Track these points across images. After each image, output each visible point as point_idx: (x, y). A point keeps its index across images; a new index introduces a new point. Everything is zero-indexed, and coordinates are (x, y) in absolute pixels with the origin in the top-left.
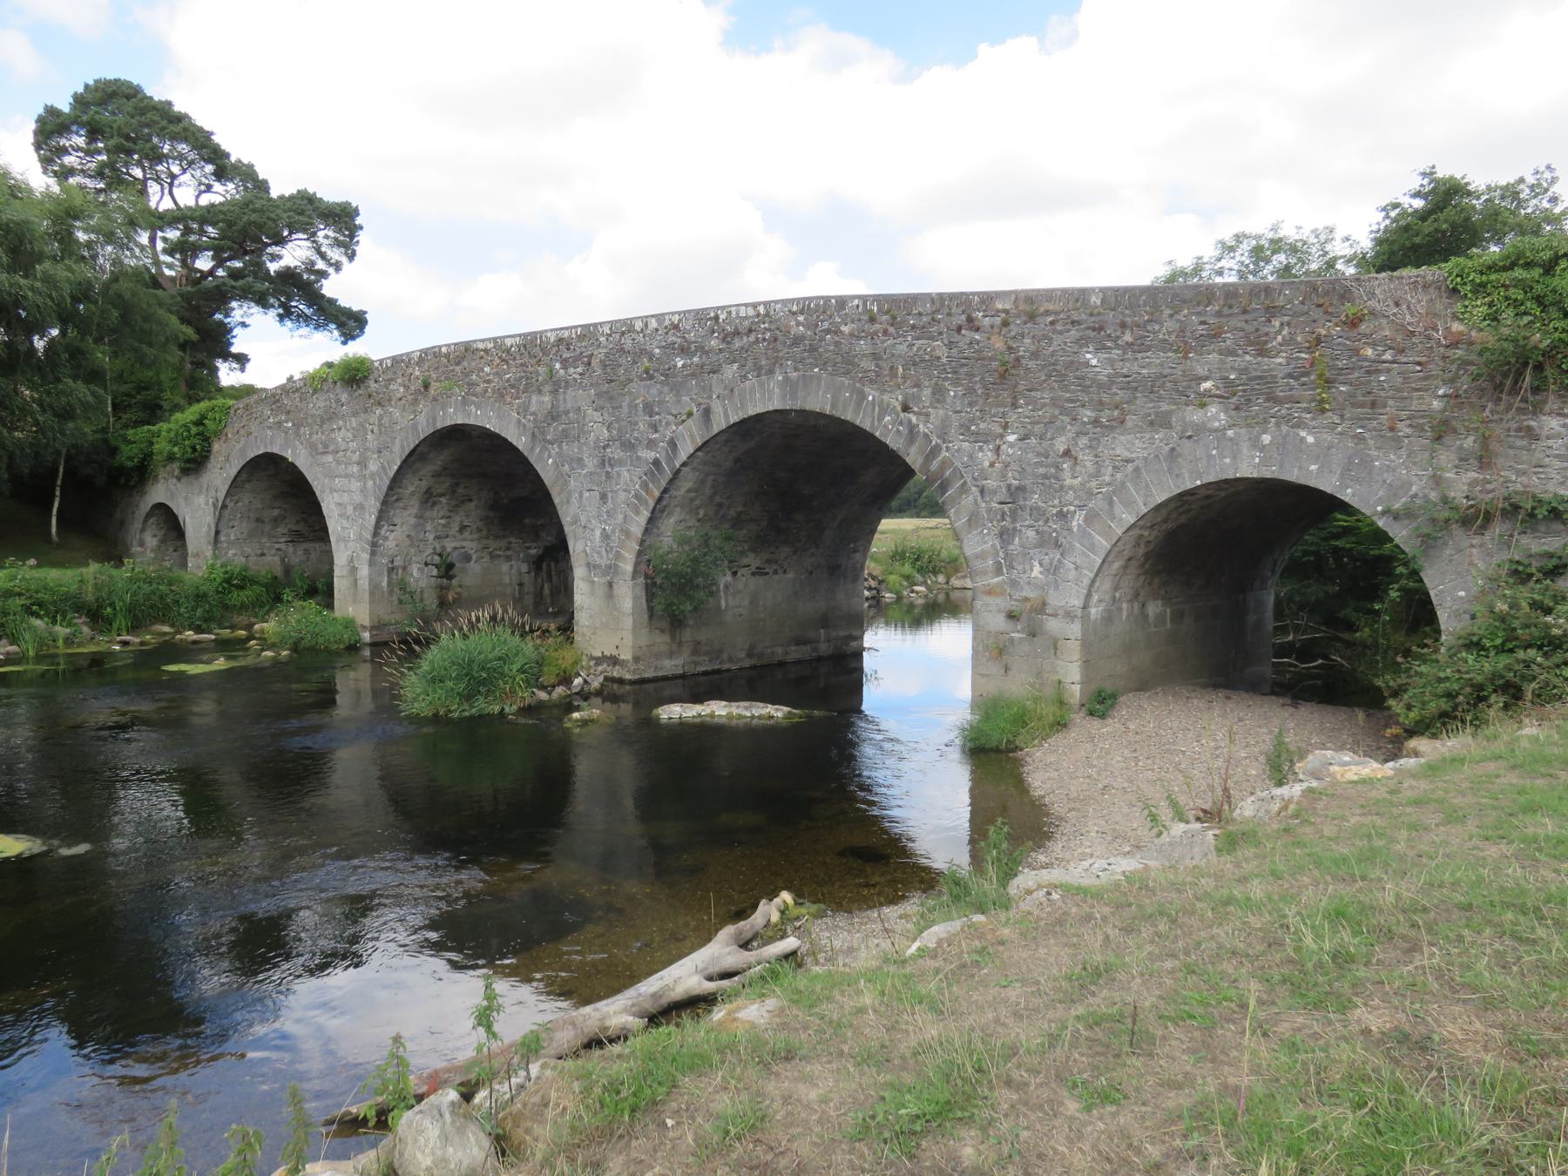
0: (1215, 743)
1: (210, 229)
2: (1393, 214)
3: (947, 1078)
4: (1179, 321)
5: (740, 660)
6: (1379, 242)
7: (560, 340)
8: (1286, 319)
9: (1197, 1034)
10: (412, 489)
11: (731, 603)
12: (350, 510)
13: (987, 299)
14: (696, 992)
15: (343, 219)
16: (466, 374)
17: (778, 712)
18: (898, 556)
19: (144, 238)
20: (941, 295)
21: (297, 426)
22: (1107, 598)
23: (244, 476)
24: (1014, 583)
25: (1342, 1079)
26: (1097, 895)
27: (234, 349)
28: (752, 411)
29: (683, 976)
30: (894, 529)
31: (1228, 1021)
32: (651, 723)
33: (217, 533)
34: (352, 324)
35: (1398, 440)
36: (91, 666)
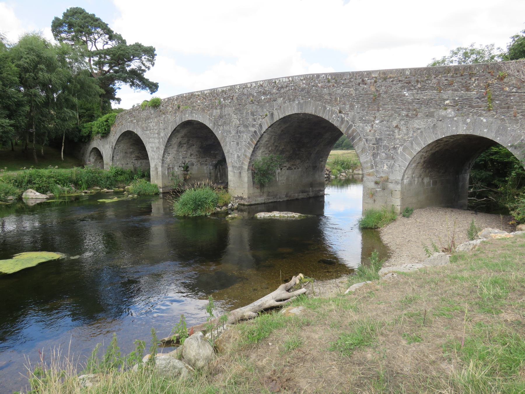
0: (450, 225)
1: (108, 57)
2: (516, 39)
3: (361, 332)
4: (437, 79)
5: (283, 198)
6: (510, 49)
7: (223, 91)
8: (477, 78)
9: (446, 320)
10: (175, 142)
11: (280, 179)
12: (155, 149)
13: (369, 73)
14: (273, 305)
15: (150, 52)
16: (192, 103)
17: (296, 215)
18: (336, 163)
19: (87, 60)
20: (353, 72)
21: (138, 121)
22: (410, 176)
23: (121, 138)
24: (377, 172)
25: (498, 336)
26: (410, 275)
27: (116, 97)
28: (287, 114)
29: (269, 300)
30: (335, 154)
31: (457, 316)
32: (254, 219)
33: (113, 157)
34: (154, 87)
35: (517, 120)
36: (75, 200)
